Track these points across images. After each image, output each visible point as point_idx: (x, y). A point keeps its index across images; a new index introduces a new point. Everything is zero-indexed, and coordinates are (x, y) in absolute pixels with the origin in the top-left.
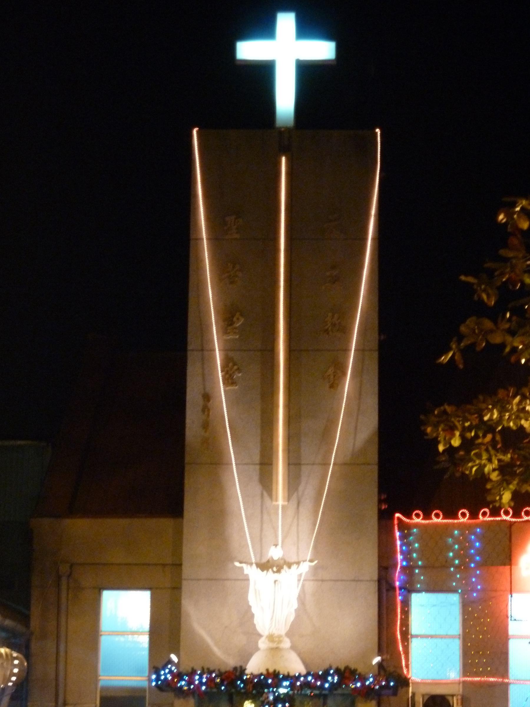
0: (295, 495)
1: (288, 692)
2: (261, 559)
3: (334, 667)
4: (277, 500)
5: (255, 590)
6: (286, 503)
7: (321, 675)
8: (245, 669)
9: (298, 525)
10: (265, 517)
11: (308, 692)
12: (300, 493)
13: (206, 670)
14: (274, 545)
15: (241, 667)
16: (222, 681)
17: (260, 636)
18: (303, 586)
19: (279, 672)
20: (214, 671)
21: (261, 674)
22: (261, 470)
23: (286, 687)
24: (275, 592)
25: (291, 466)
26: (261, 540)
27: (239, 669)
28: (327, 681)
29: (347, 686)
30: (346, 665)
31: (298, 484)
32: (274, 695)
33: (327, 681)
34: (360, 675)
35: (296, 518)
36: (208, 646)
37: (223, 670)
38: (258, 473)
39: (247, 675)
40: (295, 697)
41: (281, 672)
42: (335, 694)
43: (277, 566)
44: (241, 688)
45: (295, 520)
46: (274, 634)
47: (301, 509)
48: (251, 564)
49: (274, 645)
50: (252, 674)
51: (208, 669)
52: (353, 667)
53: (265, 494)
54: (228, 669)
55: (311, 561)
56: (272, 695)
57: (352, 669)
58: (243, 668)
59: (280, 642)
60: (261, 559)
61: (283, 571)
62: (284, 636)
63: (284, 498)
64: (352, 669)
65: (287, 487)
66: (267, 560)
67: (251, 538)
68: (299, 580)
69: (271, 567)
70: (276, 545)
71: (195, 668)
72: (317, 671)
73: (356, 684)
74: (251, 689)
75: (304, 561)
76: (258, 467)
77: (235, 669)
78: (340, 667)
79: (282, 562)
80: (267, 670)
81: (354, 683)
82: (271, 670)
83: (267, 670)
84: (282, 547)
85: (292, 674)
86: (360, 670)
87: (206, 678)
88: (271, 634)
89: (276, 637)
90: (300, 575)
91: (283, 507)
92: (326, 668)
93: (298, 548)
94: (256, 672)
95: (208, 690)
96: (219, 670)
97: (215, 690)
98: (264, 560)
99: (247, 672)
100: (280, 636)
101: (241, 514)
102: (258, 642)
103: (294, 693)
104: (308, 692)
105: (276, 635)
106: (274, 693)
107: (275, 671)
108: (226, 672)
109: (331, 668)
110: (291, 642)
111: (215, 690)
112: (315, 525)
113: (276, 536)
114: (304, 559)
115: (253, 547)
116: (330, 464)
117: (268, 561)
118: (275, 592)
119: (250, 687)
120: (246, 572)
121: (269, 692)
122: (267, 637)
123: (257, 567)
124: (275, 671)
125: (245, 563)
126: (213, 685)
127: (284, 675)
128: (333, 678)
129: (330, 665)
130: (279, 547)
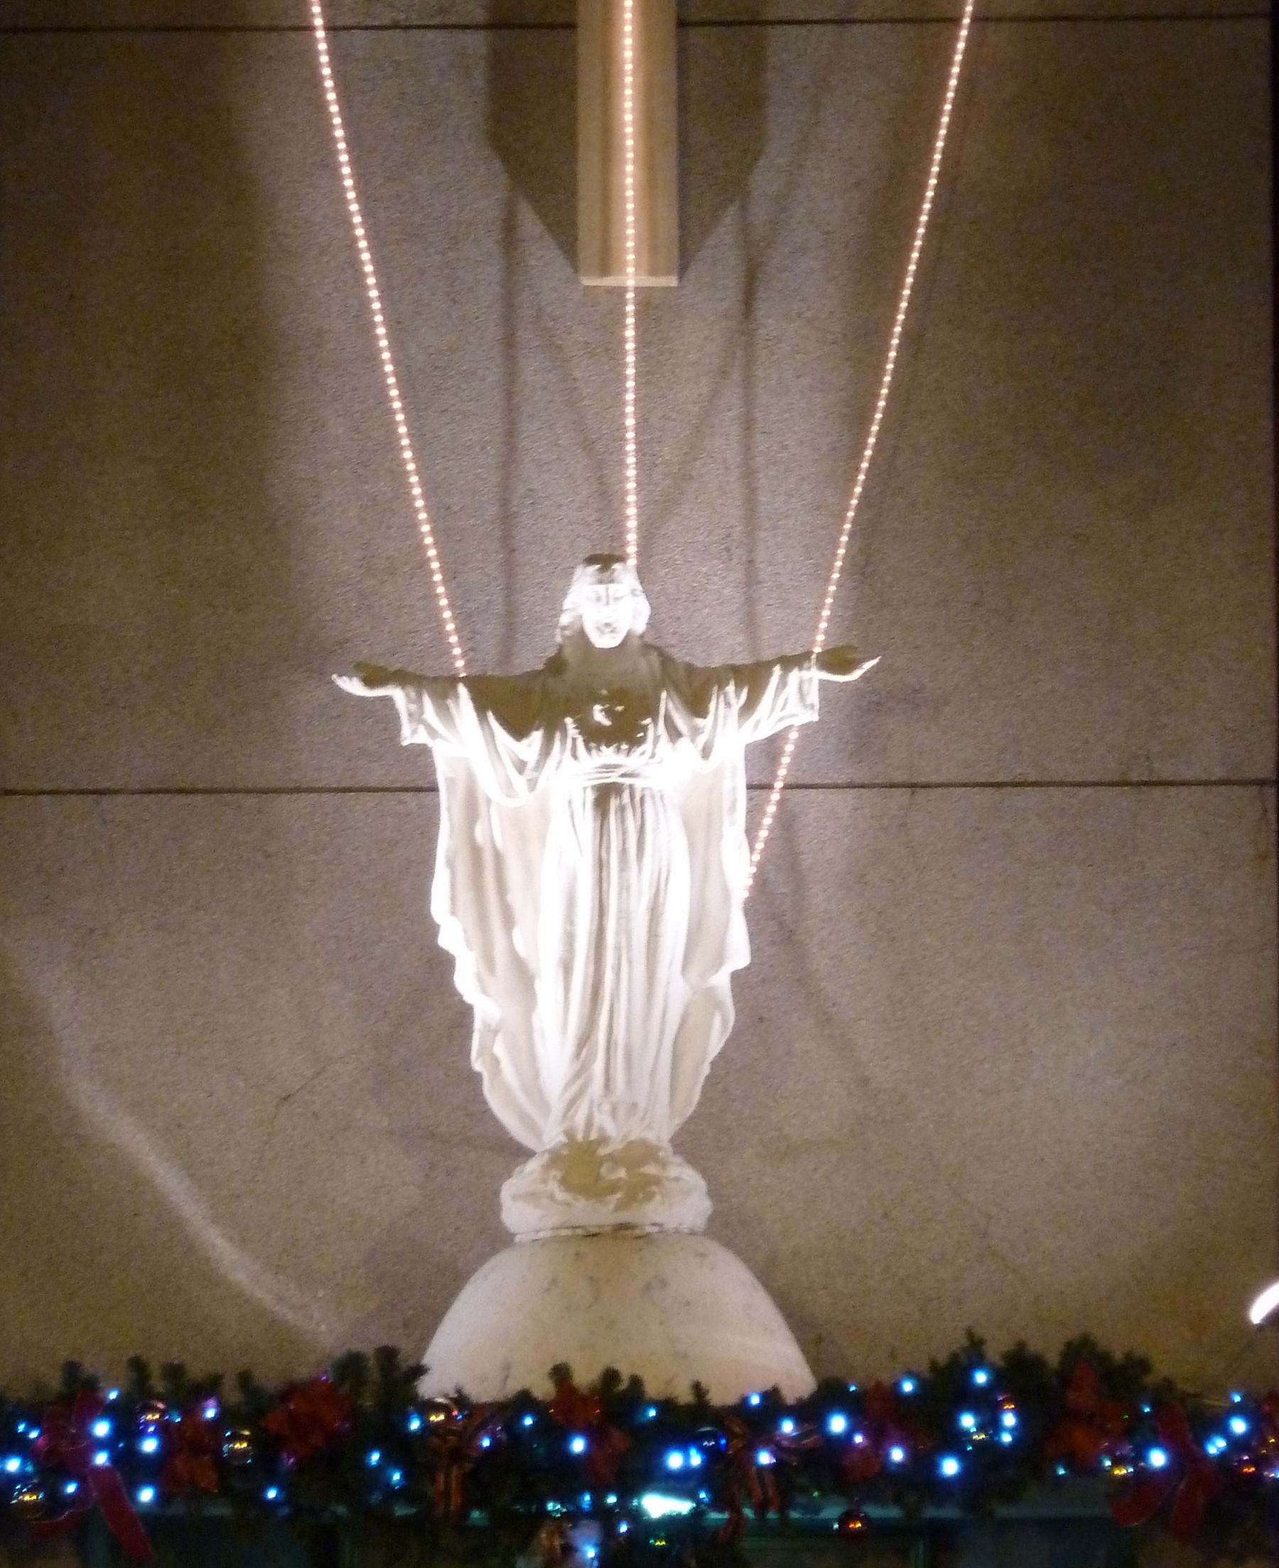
0: (726, 230)
1: (697, 1514)
2: (506, 654)
3: (996, 1349)
4: (606, 264)
5: (475, 852)
6: (672, 281)
7: (612, 721)
8: (419, 1371)
9: (748, 425)
10: (532, 368)
11: (831, 1512)
12: (760, 213)
13: (158, 1385)
14: (591, 560)
15: (388, 1355)
16: (266, 1447)
17: (518, 1153)
18: (786, 821)
19: (636, 1382)
20: (210, 1387)
21: (524, 1401)
22: (498, 63)
23: (679, 1484)
24: (572, 817)
25: (697, 37)
26: (507, 520)
27: (373, 1373)
28: (954, 1442)
29: (1085, 1468)
30: (1073, 1333)
31: (751, 154)
32: (608, 1532)
33: (954, 1442)
34: (1165, 1396)
35: (736, 376)
36: (171, 1224)
37: (269, 1377)
38: (479, 80)
39: (428, 1407)
40: (747, 1544)
41: (652, 1389)
42: (1005, 1524)
43: (617, 696)
44: (393, 1494)
45: (732, 397)
46: (603, 1140)
47: (769, 318)
48: (443, 687)
49: (604, 1214)
50: (460, 1400)
51: (174, 1372)
52: (1117, 1345)
53: (529, 222)
54: (303, 1372)
55: (836, 660)
56: (594, 1541)
57: (1118, 1356)
58: (405, 1361)
59: (641, 1189)
60: (506, 654)
61: (655, 730)
62: (666, 1151)
63: (650, 243)
64: (1118, 1356)
65: (669, 174)
66: (551, 653)
67: (439, 513)
68: (758, 787)
69: (577, 706)
70: (605, 561)
71: (91, 1365)
72: (886, 1378)
73: (1140, 1455)
74: (456, 1501)
75: (789, 663)
76: (477, 43)
77: (351, 1366)
78: (1036, 1345)
79: (647, 666)
80: (561, 1374)
81: (1127, 1449)
82: (585, 1376)
83: (561, 1374)
84: (643, 573)
85: (720, 1396)
86: (1163, 1367)
87: (164, 1430)
88: (579, 1137)
89: (614, 1159)
90: (766, 752)
91: (647, 301)
92: (942, 1358)
93: (751, 579)
94: (484, 1392)
95: (178, 1509)
96: (245, 1379)
97: (220, 1510)
98: (530, 660)
99: (428, 1387)
100: (641, 1153)
101: (372, 357)
102: (496, 1193)
103: (782, 1510)
104: (831, 1512)
105: (615, 1146)
106: (605, 1517)
107: (611, 1376)
108: (291, 1391)
109: (974, 1353)
110: (714, 1193)
111: (220, 1510)
112: (864, 419)
113: (608, 497)
114: (789, 650)
115: (450, 576)
116: (956, 21)
117: (556, 665)
118: (572, 817)
119: (448, 1481)
120: (410, 735)
121: (574, 1517)
122: (555, 1158)
123: (481, 706)
124: (611, 1376)
125: (401, 678)
126: (208, 1479)
127: (666, 1406)
128: (991, 1424)
129: (970, 1334)
130: (626, 576)
